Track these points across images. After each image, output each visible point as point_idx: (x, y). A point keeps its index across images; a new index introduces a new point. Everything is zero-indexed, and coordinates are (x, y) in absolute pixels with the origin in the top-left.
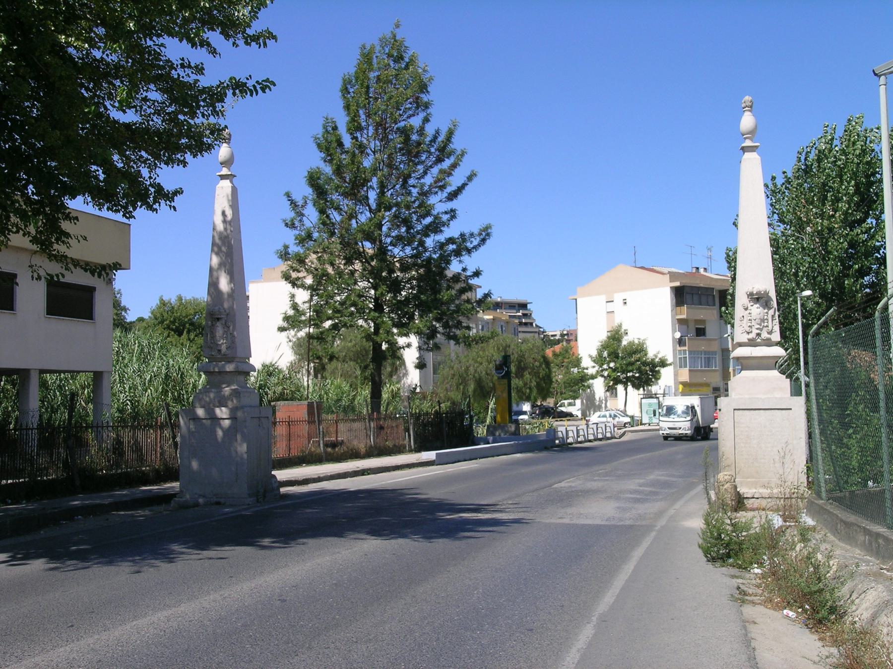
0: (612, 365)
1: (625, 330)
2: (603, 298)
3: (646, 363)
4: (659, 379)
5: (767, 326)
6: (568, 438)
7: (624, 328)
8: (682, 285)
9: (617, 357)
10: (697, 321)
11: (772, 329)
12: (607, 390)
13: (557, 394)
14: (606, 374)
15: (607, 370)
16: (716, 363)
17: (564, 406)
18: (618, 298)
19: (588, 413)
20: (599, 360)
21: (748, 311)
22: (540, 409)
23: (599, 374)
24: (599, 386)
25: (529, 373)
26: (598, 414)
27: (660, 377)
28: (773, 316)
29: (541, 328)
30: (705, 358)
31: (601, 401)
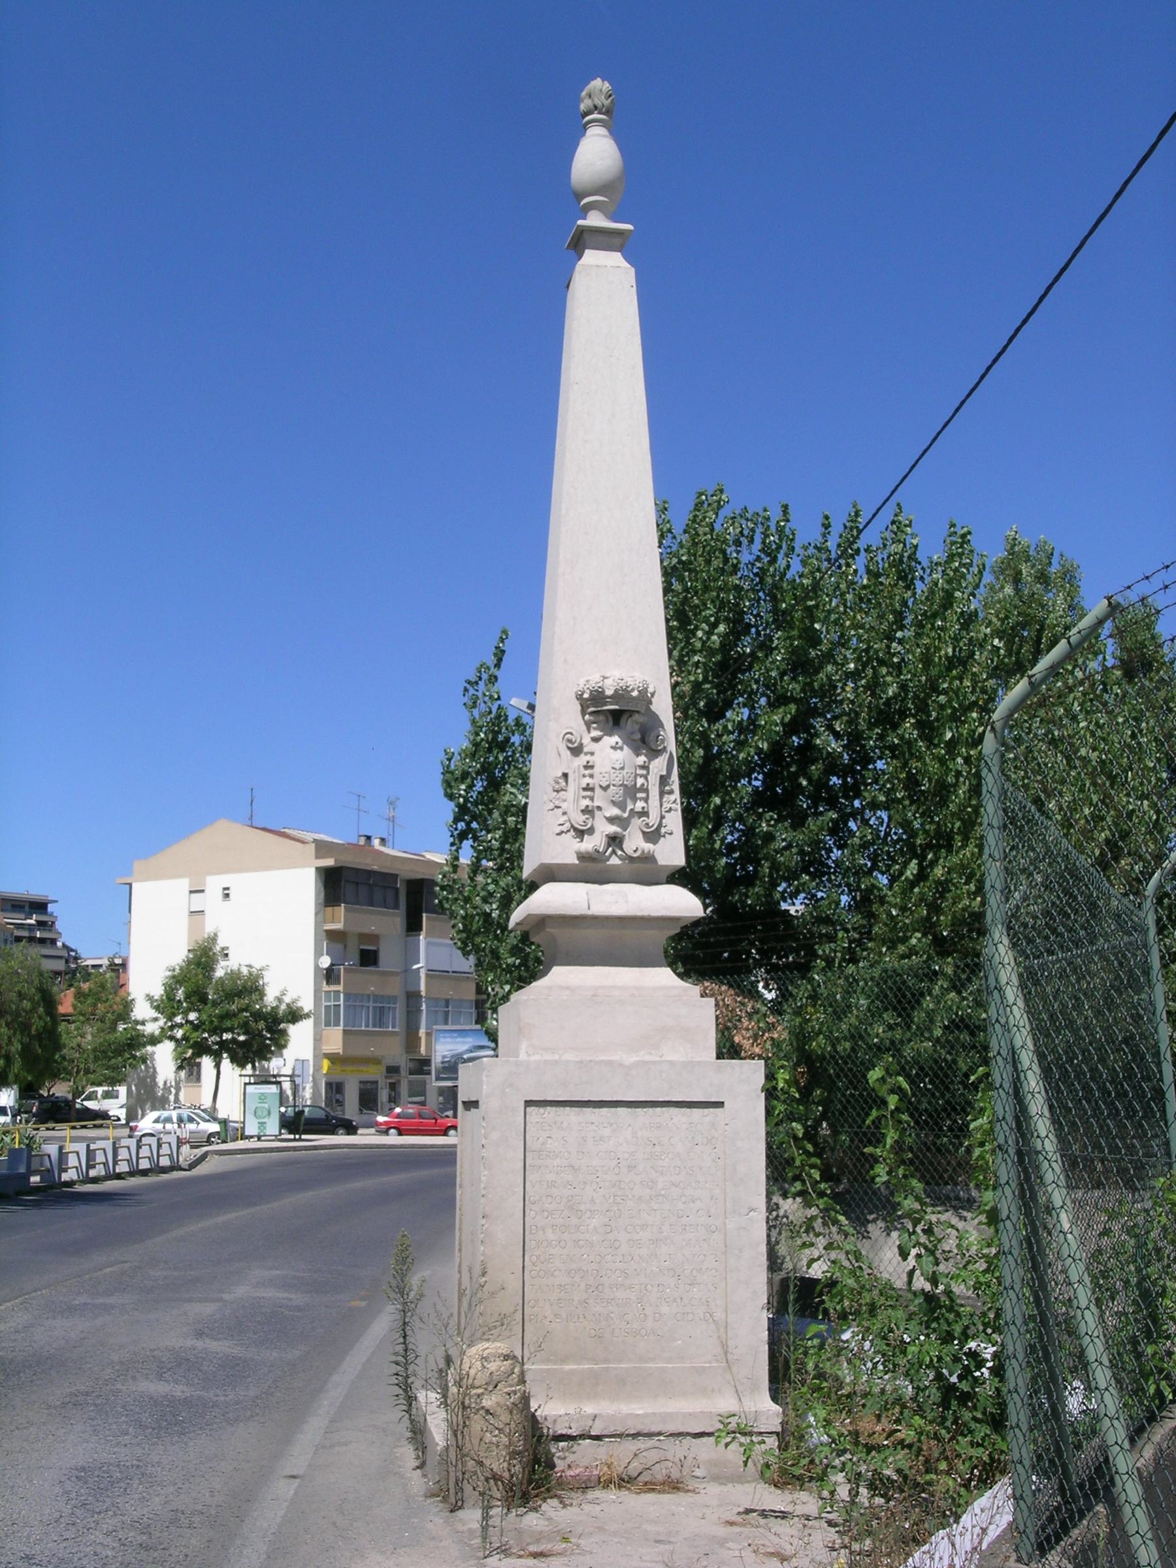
0: (192, 1016)
1: (223, 949)
2: (184, 884)
3: (259, 1016)
4: (285, 1046)
5: (644, 813)
6: (115, 1163)
7: (221, 943)
8: (339, 865)
9: (203, 999)
10: (364, 937)
11: (660, 825)
12: (180, 1068)
13: (78, 1072)
14: (179, 1033)
15: (181, 1026)
16: (394, 1018)
17: (96, 1098)
18: (214, 884)
19: (140, 1112)
20: (167, 1006)
21: (583, 759)
22: (41, 1103)
23: (166, 1034)
24: (164, 1058)
25: (7, 1025)
26: (154, 1115)
27: (287, 1041)
28: (664, 780)
29: (72, 950)
30: (374, 1007)
31: (167, 1089)
